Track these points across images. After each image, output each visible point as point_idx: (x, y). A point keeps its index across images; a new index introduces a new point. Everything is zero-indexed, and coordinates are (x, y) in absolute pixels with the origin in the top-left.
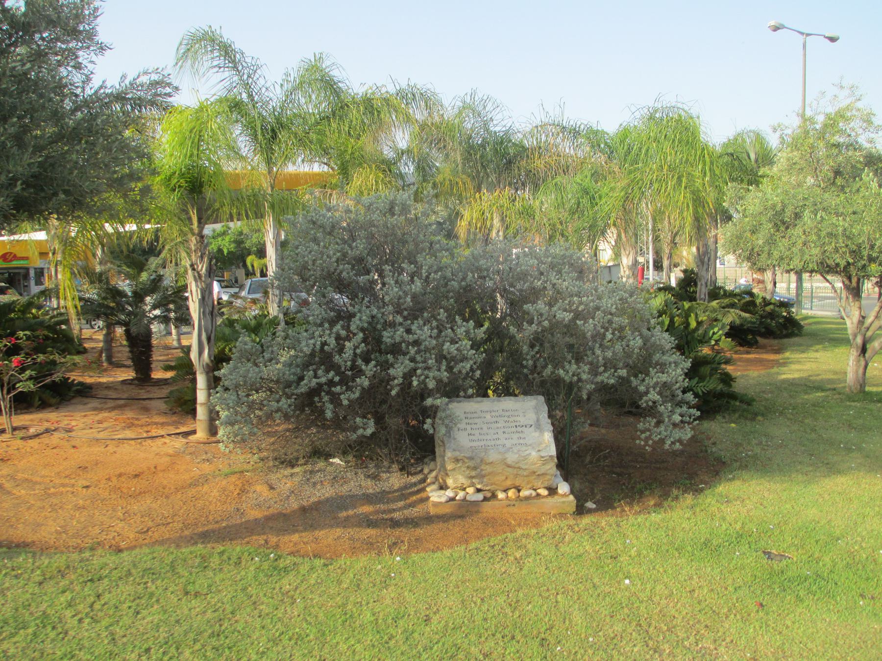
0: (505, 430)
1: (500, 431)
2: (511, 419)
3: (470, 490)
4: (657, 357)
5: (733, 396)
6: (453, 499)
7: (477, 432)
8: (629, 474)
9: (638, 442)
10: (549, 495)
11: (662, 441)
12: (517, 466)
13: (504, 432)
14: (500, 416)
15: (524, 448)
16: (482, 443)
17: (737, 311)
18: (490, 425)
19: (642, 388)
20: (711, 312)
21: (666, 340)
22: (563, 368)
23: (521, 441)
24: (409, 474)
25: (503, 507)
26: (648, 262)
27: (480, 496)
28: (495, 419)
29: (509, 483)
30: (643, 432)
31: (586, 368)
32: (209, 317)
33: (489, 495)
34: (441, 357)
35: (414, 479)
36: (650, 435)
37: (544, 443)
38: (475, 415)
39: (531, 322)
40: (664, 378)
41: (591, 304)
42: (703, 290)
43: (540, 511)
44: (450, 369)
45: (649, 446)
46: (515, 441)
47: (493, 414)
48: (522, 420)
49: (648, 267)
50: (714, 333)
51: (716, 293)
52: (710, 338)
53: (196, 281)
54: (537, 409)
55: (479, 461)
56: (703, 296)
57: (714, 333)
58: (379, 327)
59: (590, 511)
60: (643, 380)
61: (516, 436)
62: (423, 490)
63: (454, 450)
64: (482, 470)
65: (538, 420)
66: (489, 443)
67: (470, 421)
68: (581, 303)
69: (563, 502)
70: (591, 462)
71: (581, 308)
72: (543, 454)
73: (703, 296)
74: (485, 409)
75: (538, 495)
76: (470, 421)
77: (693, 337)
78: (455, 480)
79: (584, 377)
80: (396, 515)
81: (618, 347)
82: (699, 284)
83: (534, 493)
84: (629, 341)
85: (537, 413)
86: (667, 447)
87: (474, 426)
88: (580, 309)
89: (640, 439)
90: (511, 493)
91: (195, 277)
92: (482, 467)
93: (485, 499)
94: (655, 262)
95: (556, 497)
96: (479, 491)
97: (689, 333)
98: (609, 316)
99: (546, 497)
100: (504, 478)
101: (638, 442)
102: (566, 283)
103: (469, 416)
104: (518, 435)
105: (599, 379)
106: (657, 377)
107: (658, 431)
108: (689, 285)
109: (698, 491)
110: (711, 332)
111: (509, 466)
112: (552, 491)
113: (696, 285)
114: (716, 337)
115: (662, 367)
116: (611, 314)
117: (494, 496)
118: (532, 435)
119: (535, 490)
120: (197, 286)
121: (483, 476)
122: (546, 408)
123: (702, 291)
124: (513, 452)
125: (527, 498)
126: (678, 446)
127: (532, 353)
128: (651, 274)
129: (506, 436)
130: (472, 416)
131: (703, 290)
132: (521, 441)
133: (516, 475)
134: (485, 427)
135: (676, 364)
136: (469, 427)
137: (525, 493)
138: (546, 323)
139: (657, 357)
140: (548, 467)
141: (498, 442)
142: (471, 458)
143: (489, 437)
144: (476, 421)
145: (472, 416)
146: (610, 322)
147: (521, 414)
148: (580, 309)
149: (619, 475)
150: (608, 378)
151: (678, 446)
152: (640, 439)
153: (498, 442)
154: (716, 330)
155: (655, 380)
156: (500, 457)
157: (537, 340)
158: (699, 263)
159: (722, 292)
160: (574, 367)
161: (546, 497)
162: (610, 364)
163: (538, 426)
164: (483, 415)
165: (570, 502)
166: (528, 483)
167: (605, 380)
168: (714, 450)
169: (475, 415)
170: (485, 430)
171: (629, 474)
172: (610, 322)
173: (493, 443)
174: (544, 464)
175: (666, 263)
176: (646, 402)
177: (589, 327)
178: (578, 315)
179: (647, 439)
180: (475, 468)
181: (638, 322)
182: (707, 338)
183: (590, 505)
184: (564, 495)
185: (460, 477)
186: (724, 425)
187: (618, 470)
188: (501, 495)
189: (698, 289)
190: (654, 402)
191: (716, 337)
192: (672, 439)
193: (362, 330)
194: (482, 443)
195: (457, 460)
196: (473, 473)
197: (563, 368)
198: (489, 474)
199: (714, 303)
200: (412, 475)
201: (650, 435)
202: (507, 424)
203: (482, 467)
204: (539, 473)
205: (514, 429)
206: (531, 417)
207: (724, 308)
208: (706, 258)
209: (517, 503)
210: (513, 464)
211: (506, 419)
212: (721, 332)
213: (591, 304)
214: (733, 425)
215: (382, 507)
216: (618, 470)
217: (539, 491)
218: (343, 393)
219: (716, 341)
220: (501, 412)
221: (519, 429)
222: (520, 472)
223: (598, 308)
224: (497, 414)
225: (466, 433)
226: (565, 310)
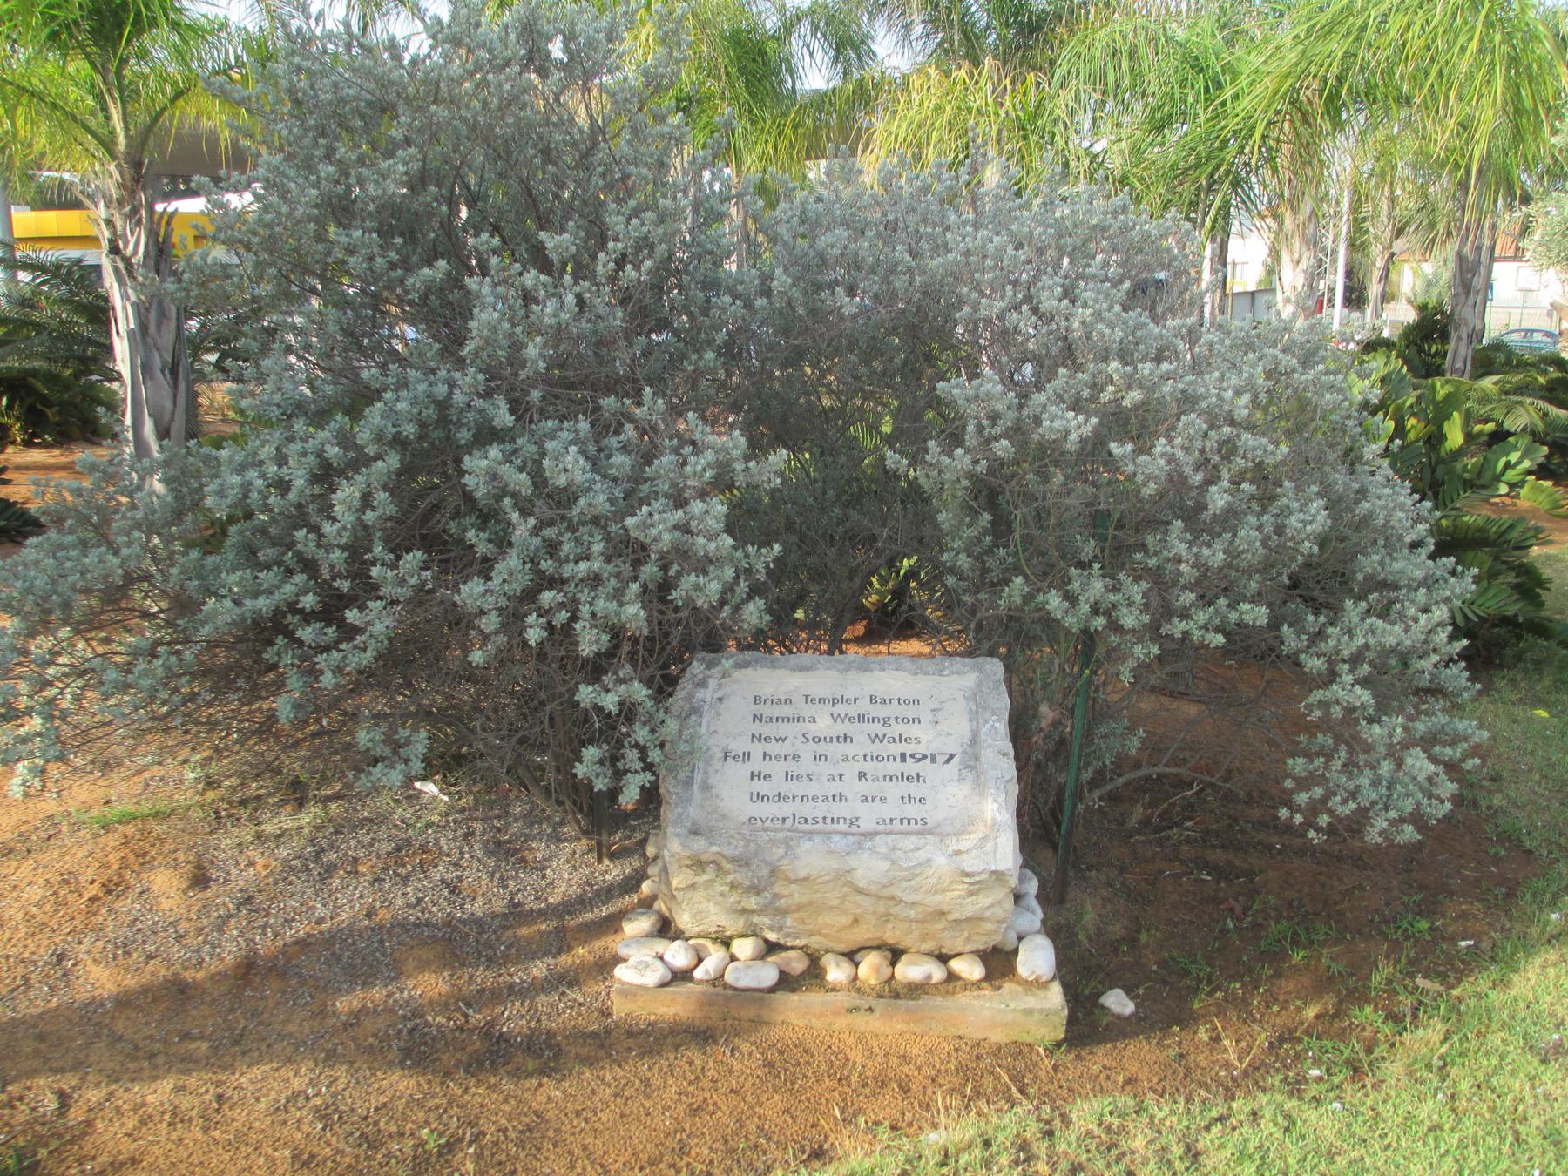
0: (868, 767)
1: (850, 771)
2: (896, 729)
3: (744, 948)
4: (1370, 563)
5: (1541, 629)
6: (681, 976)
7: (777, 769)
8: (1250, 874)
9: (1283, 813)
10: (988, 977)
11: (1362, 816)
12: (886, 892)
13: (862, 775)
14: (861, 718)
15: (913, 841)
16: (786, 809)
17: (1541, 403)
18: (822, 748)
19: (1315, 664)
20: (1479, 402)
21: (1394, 502)
22: (1063, 585)
23: (912, 810)
24: (601, 852)
25: (836, 1014)
26: (1332, 290)
27: (767, 975)
28: (841, 728)
29: (862, 935)
30: (1304, 784)
31: (1136, 591)
32: (163, 381)
33: (797, 964)
34: (632, 551)
35: (613, 872)
36: (1325, 799)
37: (972, 829)
38: (787, 710)
39: (955, 439)
40: (1391, 634)
41: (1168, 387)
42: (1463, 350)
43: (953, 1031)
44: (658, 594)
45: (1318, 829)
46: (892, 809)
47: (841, 709)
48: (926, 738)
49: (1331, 301)
50: (1508, 466)
51: (1491, 359)
52: (1497, 479)
53: (121, 283)
54: (976, 698)
55: (764, 872)
56: (1459, 365)
57: (1508, 466)
58: (464, 436)
59: (1120, 1030)
60: (1320, 635)
61: (896, 790)
62: (612, 924)
63: (695, 832)
64: (776, 896)
65: (974, 741)
66: (807, 810)
67: (766, 730)
68: (1130, 383)
69: (1028, 1012)
70: (1145, 823)
71: (1133, 397)
72: (971, 863)
73: (1459, 365)
74: (818, 691)
75: (952, 977)
76: (766, 730)
77: (1451, 472)
78: (698, 915)
79: (1129, 620)
80: (513, 1019)
81: (1249, 537)
82: (1454, 336)
83: (937, 973)
84: (1286, 512)
85: (974, 716)
86: (1373, 836)
87: (774, 748)
88: (1127, 403)
89: (1288, 804)
90: (870, 967)
91: (116, 270)
92: (777, 889)
93: (786, 982)
94: (1348, 289)
95: (1008, 986)
96: (771, 948)
97: (1441, 461)
98: (1227, 430)
99: (977, 985)
100: (846, 920)
101: (1283, 813)
102: (1096, 313)
103: (767, 710)
104: (905, 788)
105: (1177, 627)
106: (1359, 629)
107: (1351, 786)
108: (1428, 337)
109: (1453, 969)
110: (1502, 462)
111: (860, 891)
112: (999, 962)
113: (1445, 337)
114: (1511, 475)
115: (1385, 595)
116: (1232, 422)
117: (814, 972)
118: (948, 794)
119: (943, 959)
120: (124, 296)
121: (783, 912)
122: (1005, 701)
123: (1458, 351)
124: (873, 850)
125: (916, 990)
126: (1409, 833)
127: (969, 532)
128: (1336, 314)
129: (865, 787)
130: (778, 711)
131: (1463, 350)
132: (912, 810)
133: (886, 918)
134: (806, 752)
135: (1429, 583)
136: (757, 750)
137: (911, 970)
138: (1003, 448)
139: (1370, 563)
140: (984, 900)
141: (838, 809)
142: (742, 862)
143: (811, 789)
144: (785, 729)
145: (778, 711)
146: (1228, 450)
147: (926, 717)
148: (1127, 403)
149: (1220, 873)
150: (1205, 627)
151: (1409, 833)
152: (1288, 804)
153: (838, 809)
154: (1514, 457)
155: (1360, 641)
156: (833, 864)
157: (987, 492)
158: (1460, 290)
159: (1501, 357)
160: (1098, 586)
161: (977, 985)
162: (1215, 586)
163: (971, 761)
164: (808, 710)
165: (1047, 1013)
166: (924, 937)
167: (1197, 635)
168: (1497, 801)
169: (787, 710)
170: (806, 765)
171: (1250, 874)
172: (1228, 450)
173: (821, 810)
174: (971, 894)
175: (1374, 290)
176: (1324, 705)
177: (1149, 467)
178: (1119, 422)
179: (1314, 808)
180: (755, 890)
181: (1291, 412)
182: (1488, 475)
183: (1118, 1002)
184: (1038, 985)
185: (712, 908)
186: (1518, 711)
187: (1219, 856)
188: (836, 972)
189: (1451, 347)
190: (1350, 710)
191: (1511, 475)
192: (1392, 814)
193: (399, 442)
194: (786, 809)
195: (699, 864)
196: (752, 902)
197: (1063, 585)
198: (799, 908)
199: (1488, 383)
200: (613, 856)
201: (1325, 799)
202: (877, 749)
203: (777, 889)
204: (956, 915)
205: (895, 767)
206: (954, 731)
207: (1507, 393)
208: (1471, 278)
209: (880, 1005)
210: (873, 888)
211: (877, 728)
212: (1526, 464)
213: (1168, 387)
214: (1543, 714)
215: (483, 977)
216: (1219, 856)
217: (955, 965)
218: (326, 649)
219: (1512, 486)
220: (865, 707)
221: (911, 767)
222: (895, 910)
223: (1188, 401)
224: (852, 711)
225: (744, 769)
226: (1076, 406)
